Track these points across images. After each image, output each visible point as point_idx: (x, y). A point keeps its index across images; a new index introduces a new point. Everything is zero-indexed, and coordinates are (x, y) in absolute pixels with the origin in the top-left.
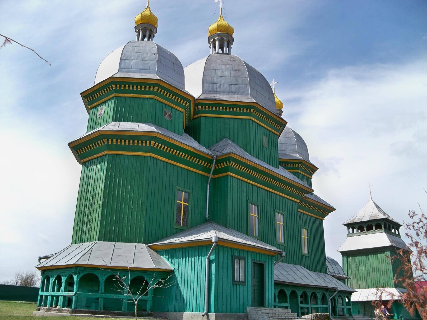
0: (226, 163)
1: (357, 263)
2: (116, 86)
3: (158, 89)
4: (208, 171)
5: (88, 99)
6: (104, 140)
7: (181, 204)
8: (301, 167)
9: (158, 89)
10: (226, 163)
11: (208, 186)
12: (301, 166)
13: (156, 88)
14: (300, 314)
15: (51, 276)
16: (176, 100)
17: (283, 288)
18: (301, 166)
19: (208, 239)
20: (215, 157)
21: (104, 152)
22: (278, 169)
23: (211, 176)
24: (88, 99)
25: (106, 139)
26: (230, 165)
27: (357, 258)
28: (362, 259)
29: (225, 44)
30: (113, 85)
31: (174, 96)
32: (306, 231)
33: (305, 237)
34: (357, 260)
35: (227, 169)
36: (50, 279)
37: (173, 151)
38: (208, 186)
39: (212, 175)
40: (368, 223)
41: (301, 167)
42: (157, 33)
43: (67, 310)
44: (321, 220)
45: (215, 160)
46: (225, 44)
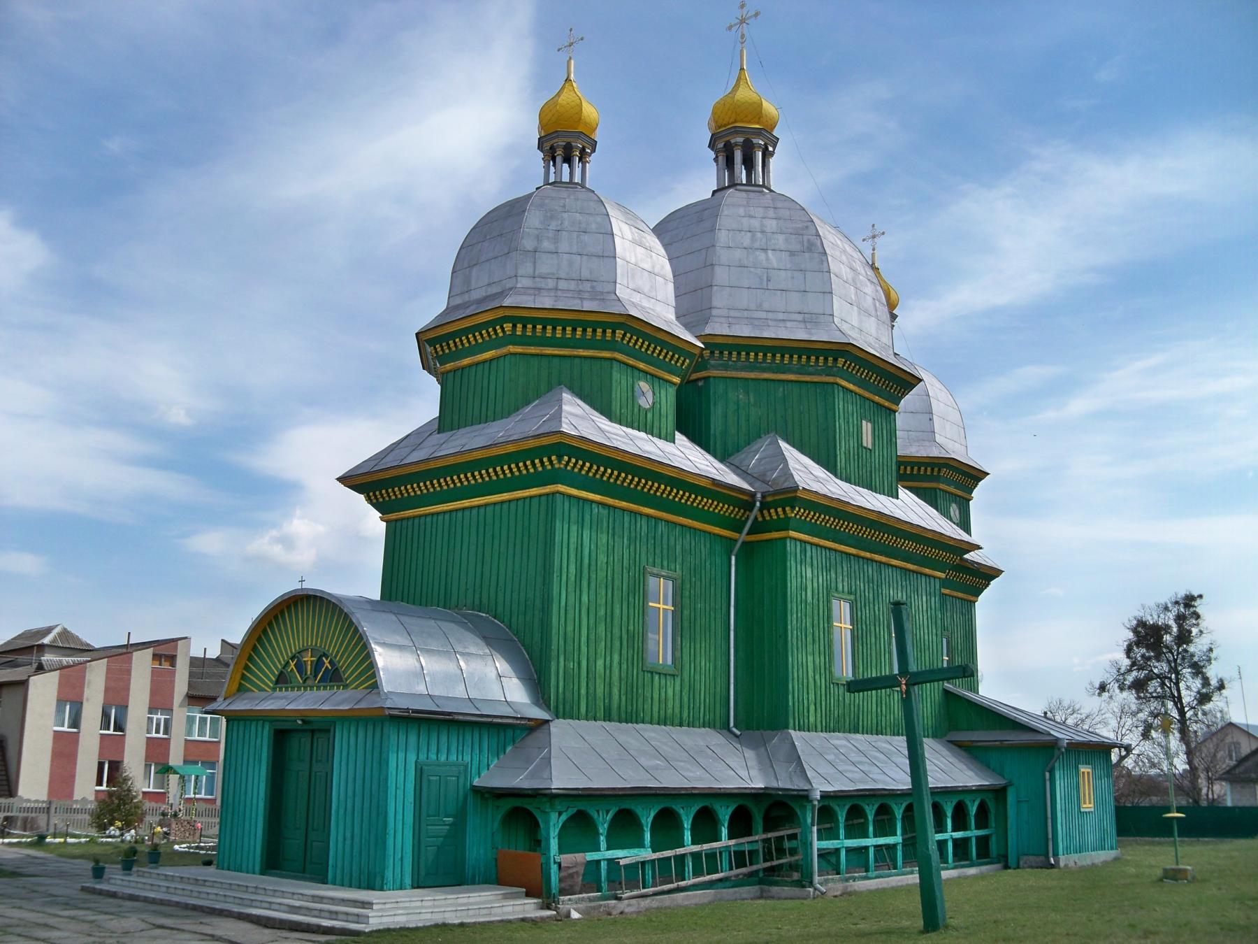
0: (784, 510)
3: (624, 335)
4: (738, 528)
5: (435, 349)
8: (844, 365)
9: (624, 335)
10: (784, 510)
11: (733, 558)
12: (845, 362)
13: (619, 333)
16: (661, 357)
18: (845, 362)
19: (988, 743)
20: (759, 495)
22: (894, 500)
23: (743, 537)
24: (435, 349)
26: (793, 515)
29: (738, 155)
30: (505, 325)
32: (845, 607)
33: (843, 625)
35: (784, 525)
38: (733, 558)
41: (844, 365)
44: (971, 601)
45: (758, 504)
46: (738, 155)
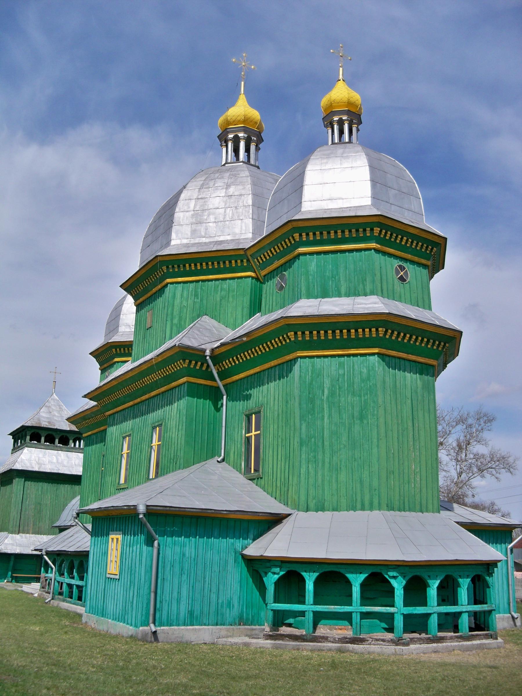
1: (40, 492)
2: (301, 235)
3: (381, 231)
6: (289, 334)
7: (252, 432)
9: (381, 231)
13: (377, 230)
14: (351, 607)
15: (429, 576)
17: (418, 574)
21: (430, 360)
25: (293, 333)
27: (41, 484)
28: (49, 488)
31: (415, 242)
34: (40, 488)
36: (459, 585)
37: (443, 346)
39: (221, 381)
40: (63, 434)
42: (361, 123)
43: (483, 635)
